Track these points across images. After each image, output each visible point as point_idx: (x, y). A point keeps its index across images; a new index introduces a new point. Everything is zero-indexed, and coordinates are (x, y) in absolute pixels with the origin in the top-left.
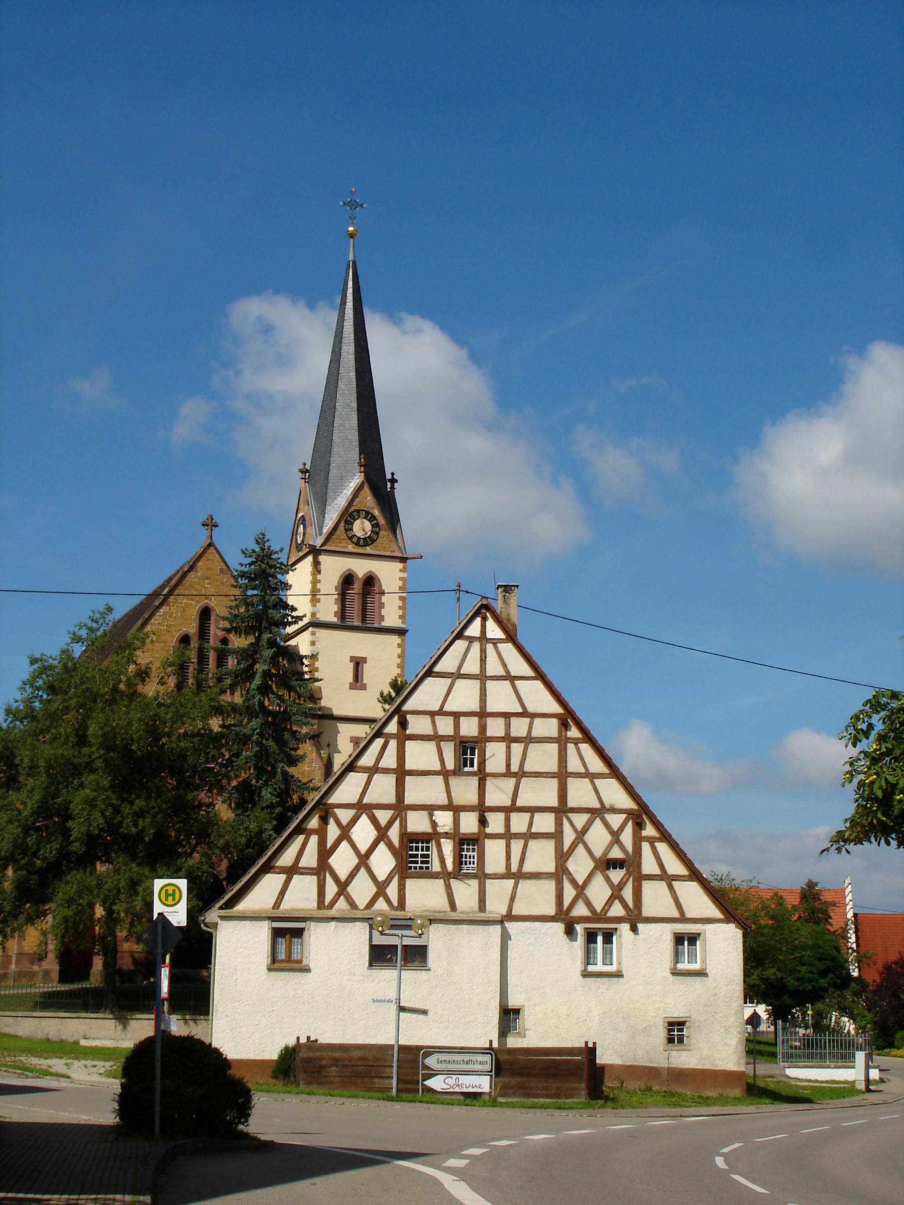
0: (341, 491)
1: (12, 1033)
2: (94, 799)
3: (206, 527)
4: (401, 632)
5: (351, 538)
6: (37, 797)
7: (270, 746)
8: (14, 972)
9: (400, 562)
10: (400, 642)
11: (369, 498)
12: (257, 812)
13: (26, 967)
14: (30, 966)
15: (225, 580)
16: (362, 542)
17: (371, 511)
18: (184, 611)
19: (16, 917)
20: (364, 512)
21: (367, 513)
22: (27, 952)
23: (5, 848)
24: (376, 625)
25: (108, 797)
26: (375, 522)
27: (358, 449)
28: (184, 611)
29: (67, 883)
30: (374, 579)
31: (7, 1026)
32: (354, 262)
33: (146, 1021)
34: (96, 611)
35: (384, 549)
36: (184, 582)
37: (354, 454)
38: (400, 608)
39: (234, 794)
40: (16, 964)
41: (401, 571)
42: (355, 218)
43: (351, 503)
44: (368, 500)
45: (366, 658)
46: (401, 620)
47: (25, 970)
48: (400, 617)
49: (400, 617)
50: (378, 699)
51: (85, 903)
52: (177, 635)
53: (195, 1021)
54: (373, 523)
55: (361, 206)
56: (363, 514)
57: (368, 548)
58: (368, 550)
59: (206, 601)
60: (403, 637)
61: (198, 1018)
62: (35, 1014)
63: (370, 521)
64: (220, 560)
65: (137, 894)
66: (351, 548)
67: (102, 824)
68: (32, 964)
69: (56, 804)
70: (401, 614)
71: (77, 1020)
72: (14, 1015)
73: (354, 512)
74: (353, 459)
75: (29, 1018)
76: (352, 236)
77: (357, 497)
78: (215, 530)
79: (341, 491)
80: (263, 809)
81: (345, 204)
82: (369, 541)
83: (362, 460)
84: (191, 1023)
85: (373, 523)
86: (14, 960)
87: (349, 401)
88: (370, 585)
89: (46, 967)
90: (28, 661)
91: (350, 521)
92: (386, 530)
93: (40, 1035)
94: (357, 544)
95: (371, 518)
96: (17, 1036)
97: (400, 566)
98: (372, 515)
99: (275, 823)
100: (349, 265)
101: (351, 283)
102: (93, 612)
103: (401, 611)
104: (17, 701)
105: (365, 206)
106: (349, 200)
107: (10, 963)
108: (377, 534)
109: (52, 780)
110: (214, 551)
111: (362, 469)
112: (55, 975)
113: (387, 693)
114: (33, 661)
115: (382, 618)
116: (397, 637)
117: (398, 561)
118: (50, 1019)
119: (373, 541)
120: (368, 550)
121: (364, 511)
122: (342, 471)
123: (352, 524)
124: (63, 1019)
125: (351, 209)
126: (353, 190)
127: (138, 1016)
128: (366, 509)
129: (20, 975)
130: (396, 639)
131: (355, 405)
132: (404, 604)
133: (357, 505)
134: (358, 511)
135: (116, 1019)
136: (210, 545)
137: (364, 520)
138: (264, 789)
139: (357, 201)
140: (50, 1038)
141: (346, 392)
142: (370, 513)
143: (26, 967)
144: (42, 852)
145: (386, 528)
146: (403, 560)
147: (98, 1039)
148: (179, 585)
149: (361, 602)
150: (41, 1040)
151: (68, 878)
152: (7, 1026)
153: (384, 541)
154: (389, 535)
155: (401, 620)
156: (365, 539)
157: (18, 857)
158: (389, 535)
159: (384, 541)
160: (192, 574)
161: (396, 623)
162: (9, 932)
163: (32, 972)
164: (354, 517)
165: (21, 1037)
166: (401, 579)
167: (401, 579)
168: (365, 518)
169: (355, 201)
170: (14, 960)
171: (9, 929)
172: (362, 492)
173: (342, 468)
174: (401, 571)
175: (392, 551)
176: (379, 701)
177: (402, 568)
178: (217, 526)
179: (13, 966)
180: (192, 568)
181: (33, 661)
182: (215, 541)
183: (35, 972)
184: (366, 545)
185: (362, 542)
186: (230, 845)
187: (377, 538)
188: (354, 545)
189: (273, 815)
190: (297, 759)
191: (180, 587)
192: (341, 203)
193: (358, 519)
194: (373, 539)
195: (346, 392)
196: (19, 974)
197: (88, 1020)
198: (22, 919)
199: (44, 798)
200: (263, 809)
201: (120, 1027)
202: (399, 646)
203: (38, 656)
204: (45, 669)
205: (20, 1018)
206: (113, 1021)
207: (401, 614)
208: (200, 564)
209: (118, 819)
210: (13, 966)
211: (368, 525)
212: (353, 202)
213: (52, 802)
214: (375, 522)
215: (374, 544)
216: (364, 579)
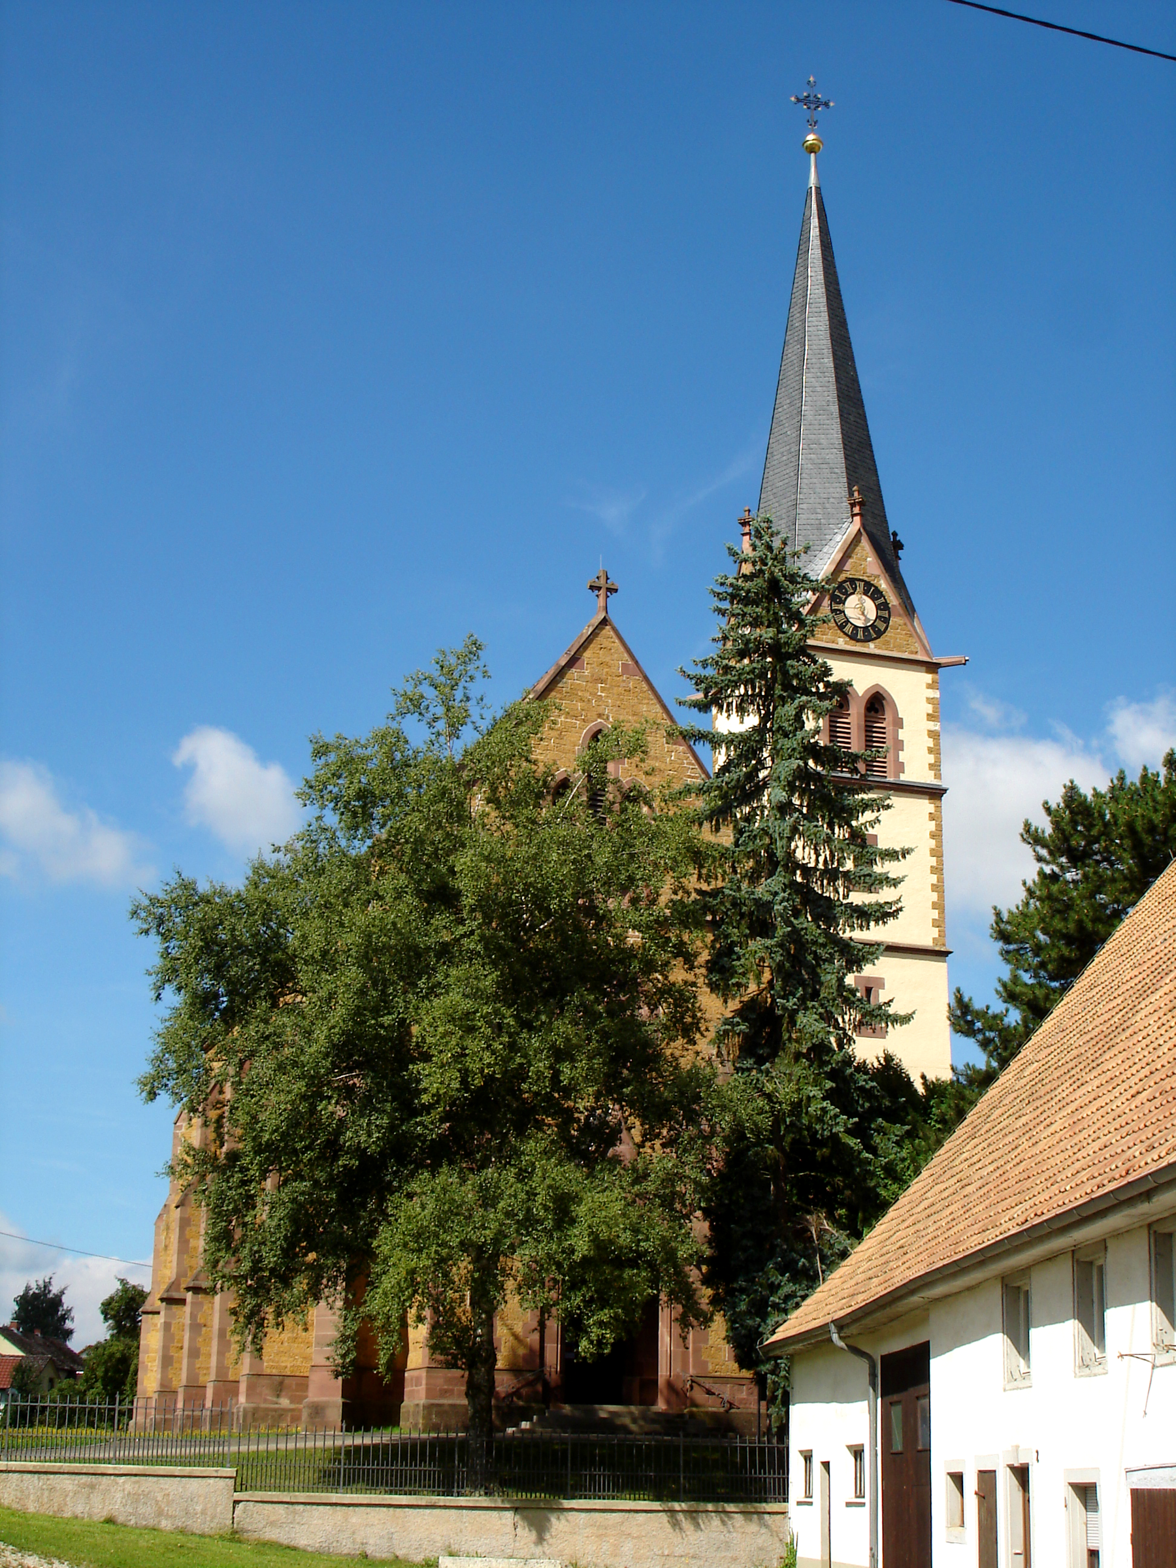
0: (819, 548)
1: (284, 1539)
2: (468, 1015)
3: (596, 592)
4: (935, 793)
5: (841, 627)
6: (338, 1014)
7: (806, 929)
8: (244, 1409)
9: (927, 672)
10: (933, 811)
11: (869, 559)
12: (782, 1064)
13: (265, 1401)
14: (275, 1399)
15: (631, 685)
16: (860, 635)
17: (875, 582)
18: (560, 737)
19: (286, 1281)
20: (862, 584)
21: (868, 585)
22: (268, 1371)
23: (271, 1125)
24: (891, 779)
25: (496, 1012)
26: (882, 600)
27: (845, 480)
28: (560, 737)
29: (410, 1196)
30: (884, 698)
31: (272, 1524)
32: (818, 189)
33: (583, 1515)
34: (448, 651)
35: (899, 648)
36: (560, 685)
37: (838, 487)
38: (930, 751)
39: (738, 1024)
40: (247, 1396)
41: (929, 686)
42: (816, 123)
43: (839, 567)
44: (868, 563)
45: (876, 836)
46: (933, 772)
47: (263, 1405)
48: (931, 767)
49: (931, 767)
50: (1022, 836)
51: (454, 1243)
52: (591, 726)
53: (691, 1514)
54: (878, 602)
55: (826, 104)
56: (860, 587)
57: (871, 645)
58: (871, 648)
59: (599, 720)
60: (938, 803)
61: (702, 1506)
62: (334, 1497)
63: (873, 599)
64: (622, 649)
65: (573, 1221)
66: (842, 643)
67: (489, 1065)
68: (278, 1396)
69: (382, 1026)
70: (933, 762)
71: (428, 1511)
72: (288, 1500)
73: (845, 582)
74: (837, 495)
75: (321, 1508)
76: (812, 149)
77: (850, 557)
78: (613, 597)
79: (819, 548)
80: (798, 1056)
81: (798, 100)
82: (872, 632)
83: (856, 494)
84: (686, 1524)
85: (878, 602)
86: (243, 1387)
87: (824, 403)
88: (877, 711)
89: (316, 1399)
90: (310, 748)
91: (840, 598)
92: (900, 615)
93: (347, 1546)
94: (853, 637)
95: (875, 593)
96: (295, 1549)
97: (928, 678)
98: (876, 588)
99: (829, 1084)
100: (809, 194)
101: (816, 220)
102: (444, 653)
103: (932, 756)
104: (277, 850)
105: (831, 104)
106: (805, 94)
107: (236, 1393)
108: (886, 621)
109: (378, 980)
110: (612, 633)
111: (856, 510)
112: (335, 1414)
113: (1092, 792)
114: (321, 751)
115: (900, 767)
116: (927, 801)
117: (924, 668)
118: (369, 1509)
119: (880, 634)
120: (871, 648)
121: (862, 580)
122: (820, 516)
123: (848, 596)
124: (398, 1510)
125: (809, 108)
126: (811, 79)
127: (567, 1504)
128: (866, 579)
129: (255, 1416)
130: (925, 806)
131: (835, 409)
132: (937, 744)
133: (850, 570)
134: (852, 581)
135: (516, 1510)
136: (604, 622)
137: (864, 597)
138: (800, 1014)
139: (819, 96)
140: (369, 1552)
141: (819, 389)
142: (873, 585)
143: (265, 1401)
144: (349, 1134)
145: (901, 612)
146: (932, 667)
147: (477, 1555)
148: (552, 690)
149: (863, 738)
150: (350, 1556)
151: (414, 1186)
152: (272, 1524)
153: (899, 634)
154: (905, 624)
155: (933, 773)
156: (865, 629)
157: (299, 1146)
158: (905, 624)
159: (899, 634)
160: (573, 672)
161: (927, 778)
162: (270, 1317)
163: (275, 1410)
164: (847, 591)
165: (305, 1551)
166: (930, 700)
167: (930, 700)
168: (865, 593)
169: (815, 96)
170: (243, 1387)
171: (270, 1309)
172: (858, 548)
173: (819, 511)
174: (929, 686)
175: (912, 653)
176: (1024, 840)
177: (930, 682)
178: (616, 591)
179: (242, 1399)
180: (573, 661)
181: (321, 751)
182: (612, 617)
183: (284, 1410)
184: (868, 639)
185: (860, 635)
186: (743, 1127)
187: (886, 628)
188: (848, 639)
189: (828, 1069)
190: (863, 957)
191: (553, 694)
192: (793, 99)
193: (853, 593)
194: (879, 630)
195: (819, 389)
196: (254, 1414)
197: (453, 1511)
198: (301, 1284)
199: (358, 1011)
200: (798, 1056)
201: (527, 1535)
202: (932, 817)
203: (330, 739)
204: (349, 764)
205: (301, 1507)
206: (509, 1515)
207: (933, 762)
208: (587, 655)
209: (518, 1060)
210: (242, 1399)
211: (870, 607)
212: (812, 106)
213: (373, 1022)
214: (882, 600)
215: (881, 639)
216: (867, 697)
